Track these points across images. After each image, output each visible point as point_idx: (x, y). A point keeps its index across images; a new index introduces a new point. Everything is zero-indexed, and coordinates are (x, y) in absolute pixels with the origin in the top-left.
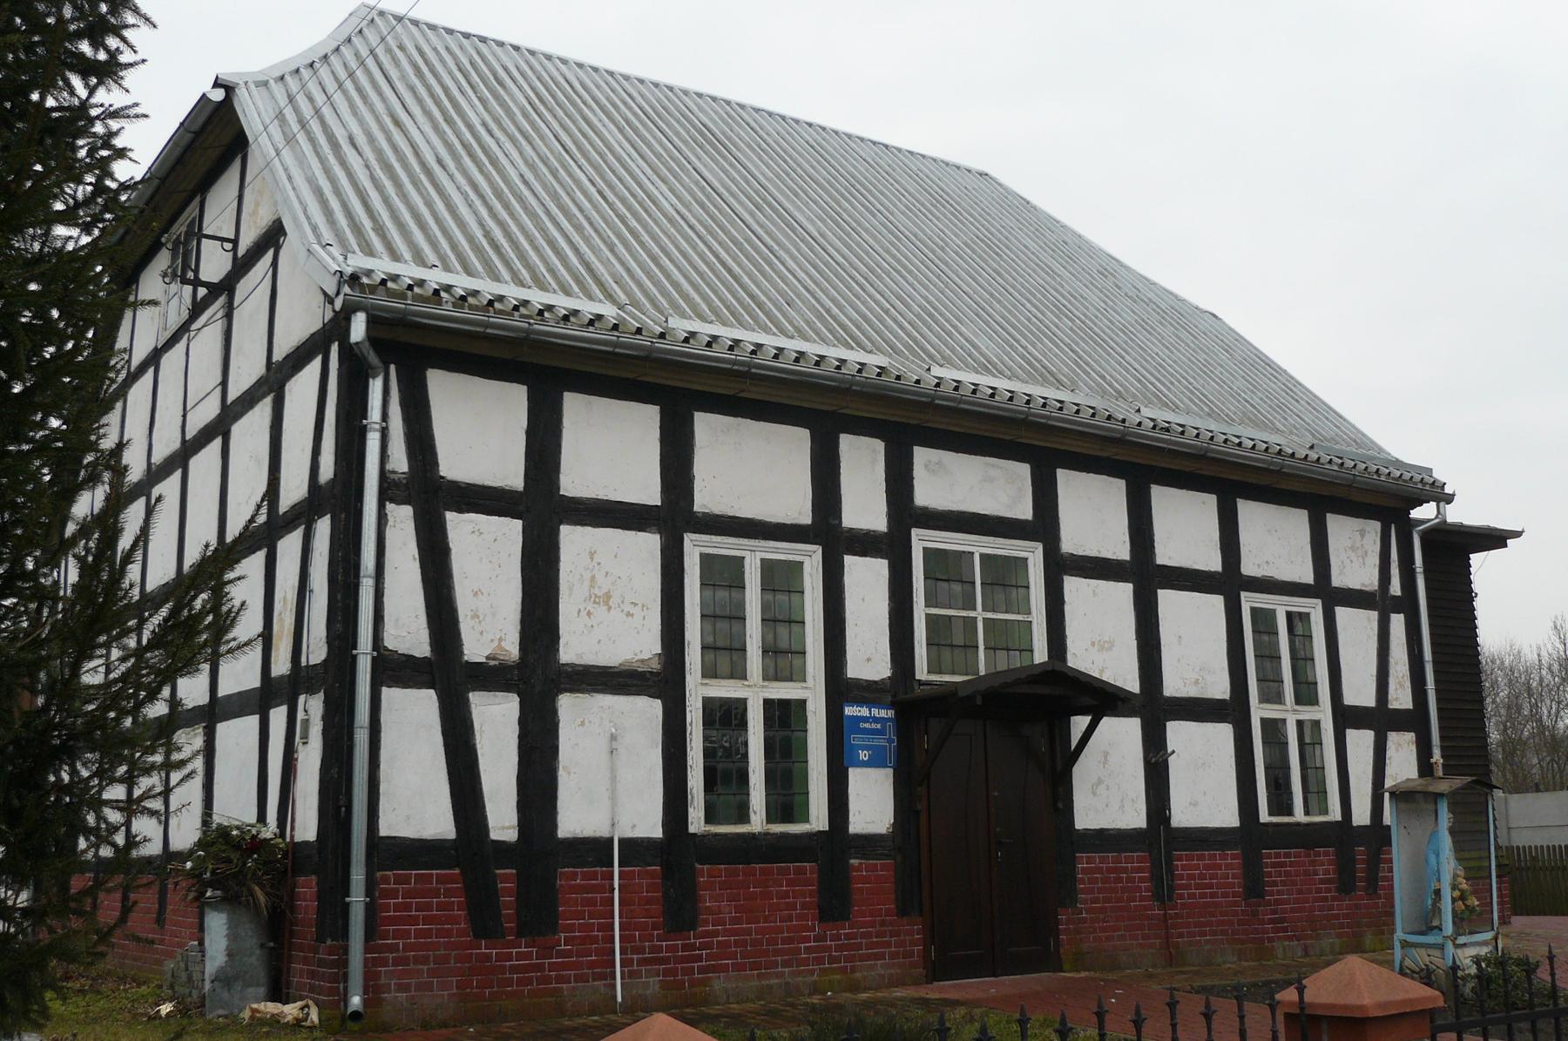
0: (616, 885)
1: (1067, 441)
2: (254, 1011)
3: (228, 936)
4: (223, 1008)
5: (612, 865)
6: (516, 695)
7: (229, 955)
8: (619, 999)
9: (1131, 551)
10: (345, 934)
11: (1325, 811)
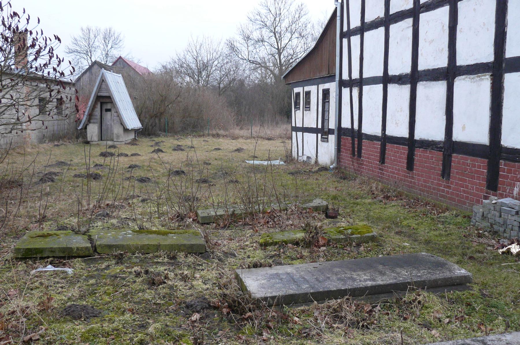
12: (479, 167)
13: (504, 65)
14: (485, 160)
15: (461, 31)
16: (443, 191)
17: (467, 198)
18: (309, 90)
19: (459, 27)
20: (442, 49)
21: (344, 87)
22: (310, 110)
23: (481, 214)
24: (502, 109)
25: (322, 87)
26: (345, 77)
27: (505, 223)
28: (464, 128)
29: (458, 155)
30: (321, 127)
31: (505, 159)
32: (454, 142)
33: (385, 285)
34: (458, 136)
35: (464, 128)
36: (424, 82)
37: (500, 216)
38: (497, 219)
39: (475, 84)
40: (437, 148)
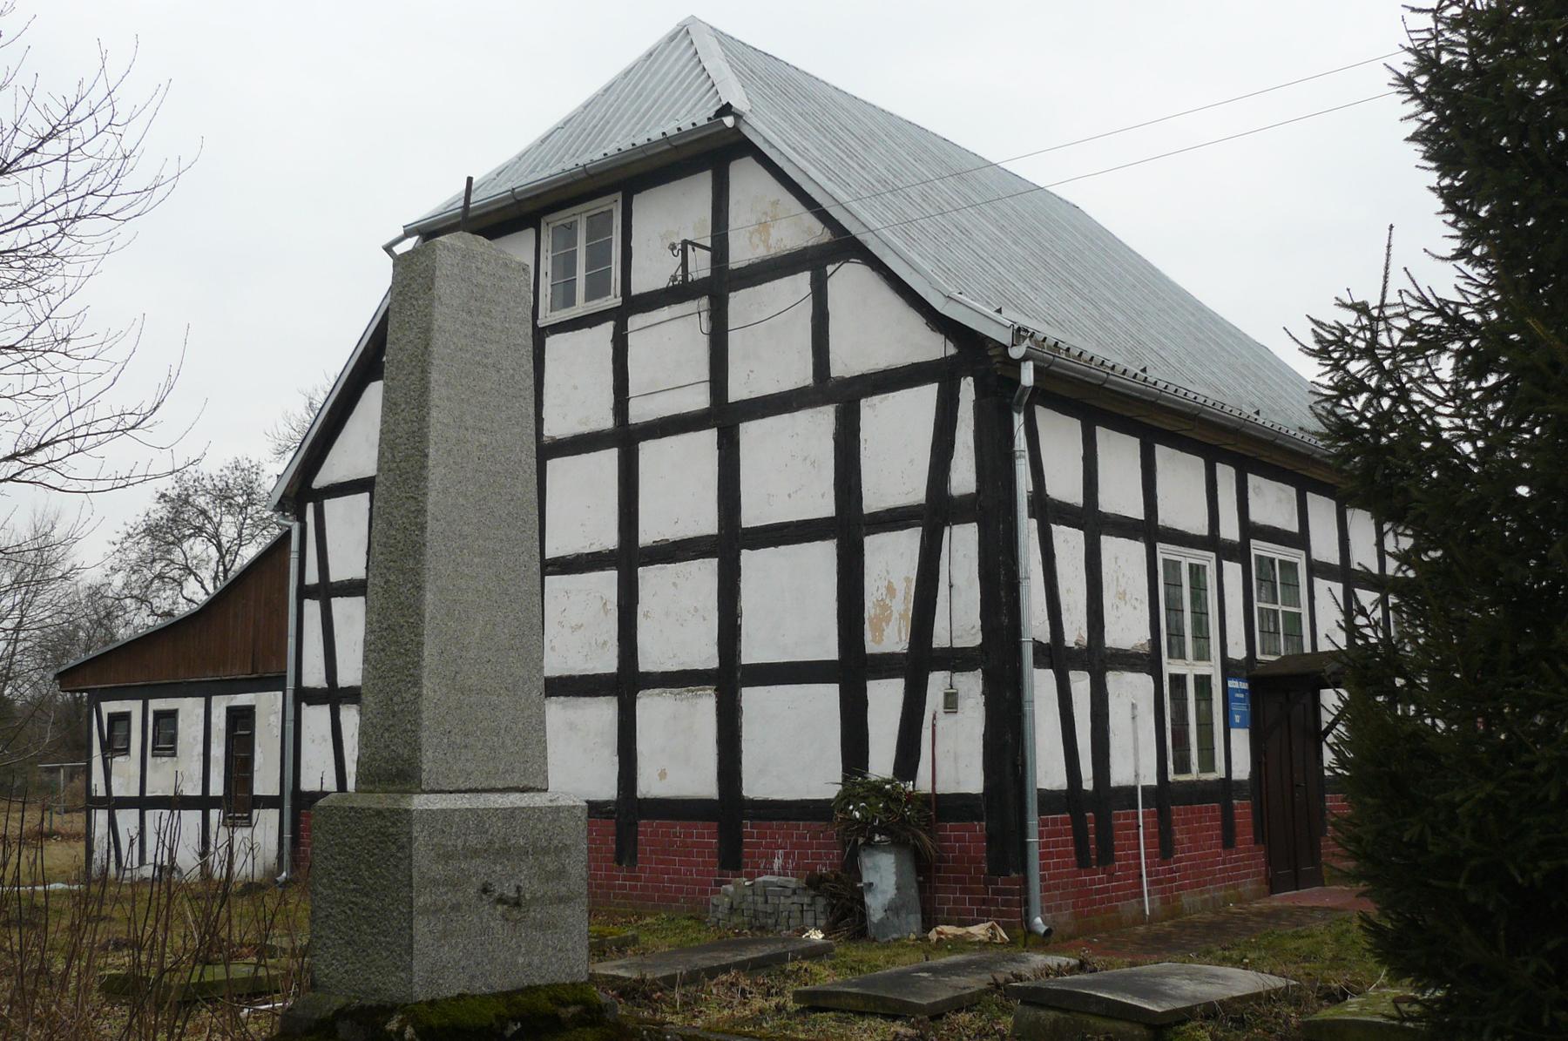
0: (1141, 824)
1: (1319, 472)
2: (941, 933)
3: (896, 874)
4: (896, 932)
5: (1137, 808)
6: (1087, 673)
7: (897, 889)
8: (1148, 913)
9: (1341, 558)
10: (1023, 867)
11: (1212, 769)
12: (701, 836)
13: (739, 675)
14: (713, 823)
15: (646, 616)
16: (622, 887)
17: (680, 890)
18: (175, 707)
19: (641, 609)
20: (605, 643)
21: (309, 704)
22: (174, 755)
23: (727, 906)
24: (741, 742)
25: (156, 704)
26: (314, 676)
27: (776, 913)
28: (663, 775)
29: (651, 821)
30: (221, 793)
31: (751, 818)
32: (639, 800)
33: (762, 957)
34: (649, 785)
35: (663, 775)
36: (562, 698)
37: (766, 902)
38: (760, 907)
39: (684, 703)
40: (601, 813)
